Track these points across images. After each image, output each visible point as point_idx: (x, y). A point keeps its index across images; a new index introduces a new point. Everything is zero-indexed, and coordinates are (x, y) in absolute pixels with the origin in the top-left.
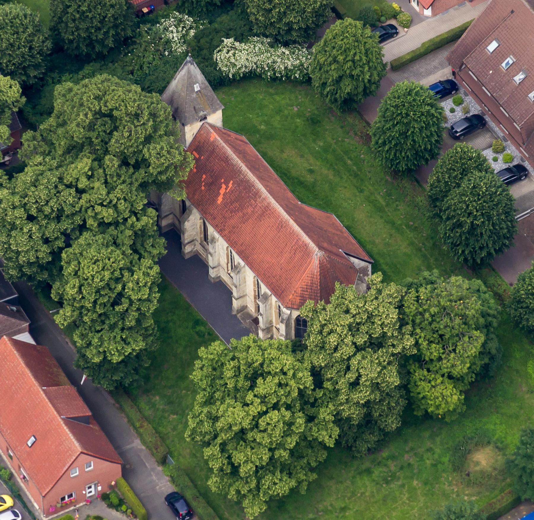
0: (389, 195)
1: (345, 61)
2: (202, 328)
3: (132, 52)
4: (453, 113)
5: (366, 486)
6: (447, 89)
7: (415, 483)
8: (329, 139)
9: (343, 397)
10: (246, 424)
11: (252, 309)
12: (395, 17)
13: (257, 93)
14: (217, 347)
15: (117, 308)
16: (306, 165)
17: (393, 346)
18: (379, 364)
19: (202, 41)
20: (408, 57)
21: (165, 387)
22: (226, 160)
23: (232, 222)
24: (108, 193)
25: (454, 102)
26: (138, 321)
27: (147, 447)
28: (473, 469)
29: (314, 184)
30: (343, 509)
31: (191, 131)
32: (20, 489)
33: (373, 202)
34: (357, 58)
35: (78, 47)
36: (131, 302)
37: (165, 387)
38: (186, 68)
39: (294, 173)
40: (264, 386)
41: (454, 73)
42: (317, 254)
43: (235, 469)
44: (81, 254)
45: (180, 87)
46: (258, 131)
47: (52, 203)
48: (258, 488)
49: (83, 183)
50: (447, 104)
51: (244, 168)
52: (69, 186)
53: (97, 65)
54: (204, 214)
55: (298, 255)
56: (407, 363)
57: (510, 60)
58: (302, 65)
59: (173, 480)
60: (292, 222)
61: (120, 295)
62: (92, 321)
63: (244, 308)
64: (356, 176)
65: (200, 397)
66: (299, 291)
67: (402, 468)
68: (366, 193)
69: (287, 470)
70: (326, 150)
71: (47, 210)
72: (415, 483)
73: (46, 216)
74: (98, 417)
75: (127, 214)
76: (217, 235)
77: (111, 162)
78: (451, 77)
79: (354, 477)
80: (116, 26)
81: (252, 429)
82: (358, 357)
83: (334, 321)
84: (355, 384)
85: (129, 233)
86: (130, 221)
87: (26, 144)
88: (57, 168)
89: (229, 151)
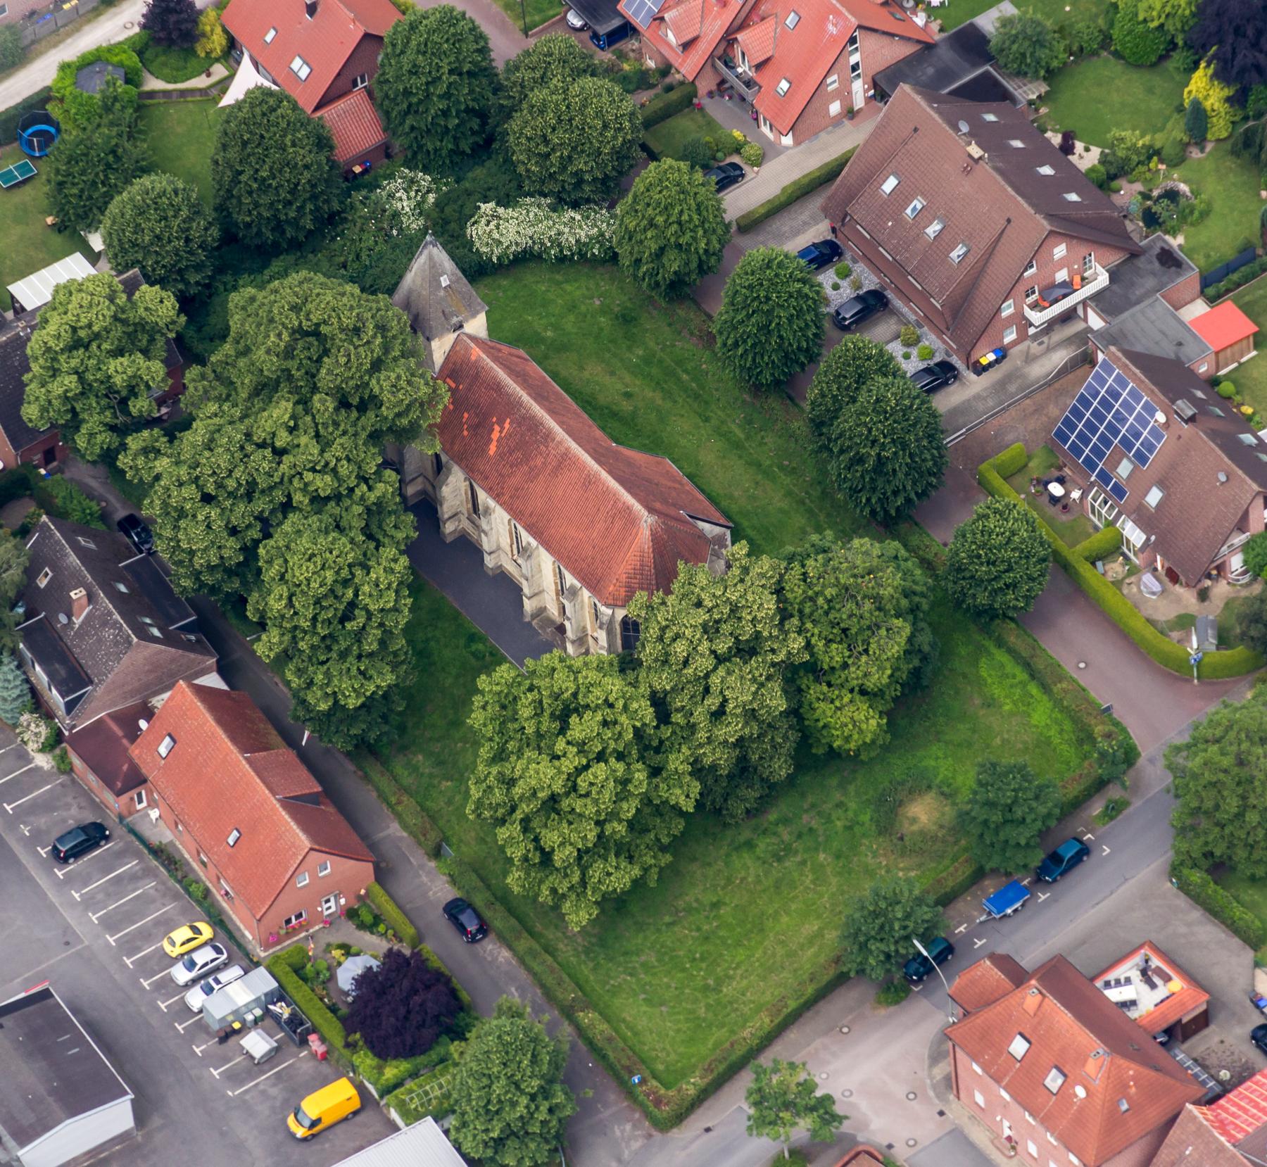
0: (750, 422)
1: (668, 224)
2: (481, 646)
3: (342, 234)
4: (836, 290)
5: (747, 867)
6: (825, 255)
7: (822, 856)
8: (652, 344)
9: (702, 735)
10: (558, 787)
11: (553, 611)
12: (738, 151)
13: (537, 282)
14: (504, 673)
15: (348, 626)
16: (619, 386)
17: (773, 651)
18: (754, 680)
19: (448, 210)
20: (762, 211)
21: (431, 739)
22: (498, 387)
23: (515, 481)
24: (322, 451)
25: (838, 274)
26: (382, 643)
27: (411, 833)
28: (907, 829)
29: (634, 414)
30: (715, 905)
31: (440, 348)
32: (221, 911)
33: (725, 435)
34: (685, 217)
35: (259, 233)
36: (369, 615)
37: (431, 739)
38: (426, 252)
39: (602, 400)
40: (581, 728)
41: (834, 230)
42: (646, 520)
43: (546, 857)
44: (288, 547)
45: (419, 282)
46: (543, 340)
47: (237, 474)
48: (583, 882)
49: (283, 439)
50: (827, 278)
51: (526, 398)
52: (262, 445)
53: (291, 258)
54: (470, 472)
55: (618, 525)
56: (796, 675)
57: (918, 204)
58: (602, 235)
59: (453, 880)
60: (604, 475)
61: (352, 605)
62: (312, 647)
63: (542, 610)
64: (697, 397)
65: (485, 752)
66: (623, 578)
67: (800, 836)
68: (714, 422)
69: (626, 851)
70: (647, 361)
71: (231, 484)
72: (822, 856)
73: (230, 494)
74: (331, 793)
75: (352, 482)
76: (492, 503)
77: (323, 404)
78: (830, 237)
79: (728, 855)
80: (314, 197)
81: (567, 794)
82: (721, 672)
83: (680, 620)
84: (718, 714)
85: (358, 509)
86: (358, 492)
87: (191, 387)
88: (241, 419)
89: (502, 374)
